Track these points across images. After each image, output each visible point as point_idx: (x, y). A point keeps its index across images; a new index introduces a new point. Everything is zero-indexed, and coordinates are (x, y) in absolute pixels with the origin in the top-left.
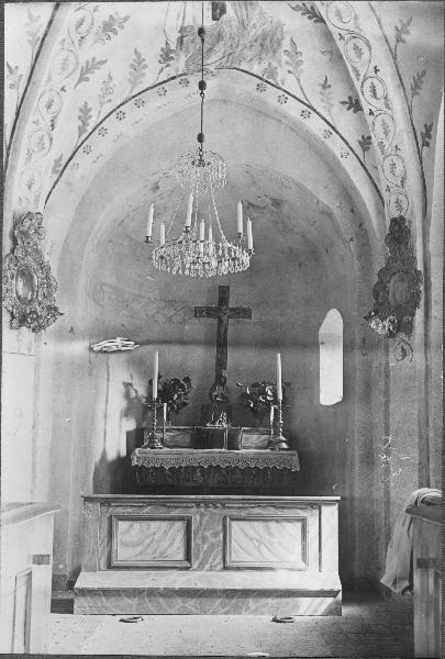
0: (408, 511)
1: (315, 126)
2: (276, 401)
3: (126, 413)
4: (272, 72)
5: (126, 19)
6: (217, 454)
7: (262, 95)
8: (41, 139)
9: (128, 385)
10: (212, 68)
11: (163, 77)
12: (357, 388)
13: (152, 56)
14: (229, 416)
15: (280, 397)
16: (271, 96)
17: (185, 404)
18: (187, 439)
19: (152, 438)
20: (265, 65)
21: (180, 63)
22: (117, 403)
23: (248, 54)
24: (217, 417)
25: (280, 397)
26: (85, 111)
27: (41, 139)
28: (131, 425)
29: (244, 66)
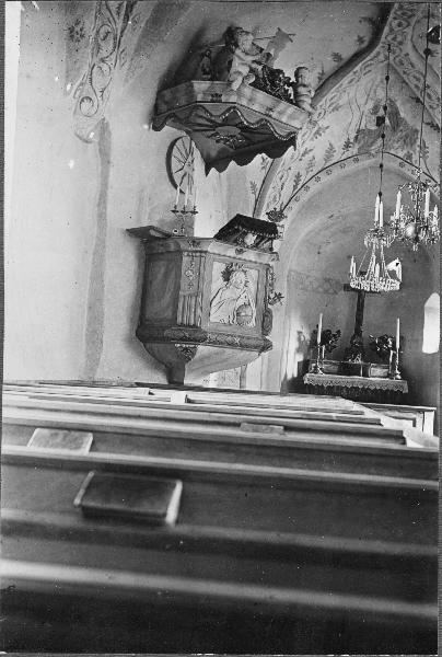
0: (392, 103)
2: (394, 348)
3: (298, 350)
4: (409, 156)
5: (327, 128)
6: (357, 380)
7: (403, 169)
8: (275, 197)
9: (299, 333)
10: (373, 152)
11: (344, 157)
12: (154, 532)
13: (339, 145)
14: (363, 356)
15: (398, 346)
16: (407, 170)
17: (335, 347)
18: (336, 369)
19: (316, 367)
20: (405, 152)
21: (354, 150)
22: (294, 344)
23: (396, 145)
24: (355, 356)
25: (398, 346)
26: (298, 176)
27: (275, 197)
28: (300, 358)
29: (392, 152)
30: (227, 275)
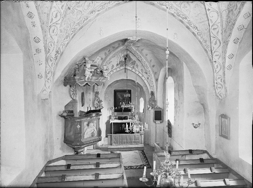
1: (140, 75)
4: (134, 67)
20: (132, 66)
30: (88, 125)
